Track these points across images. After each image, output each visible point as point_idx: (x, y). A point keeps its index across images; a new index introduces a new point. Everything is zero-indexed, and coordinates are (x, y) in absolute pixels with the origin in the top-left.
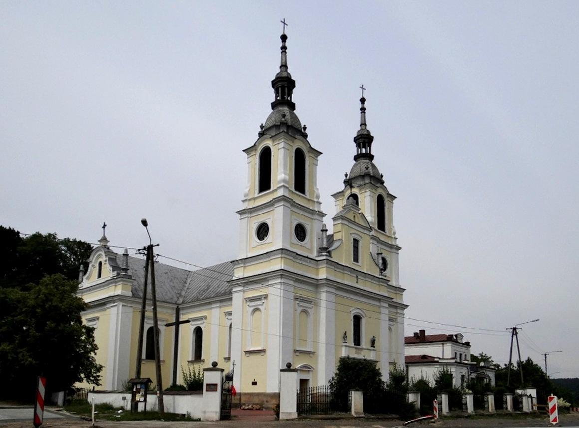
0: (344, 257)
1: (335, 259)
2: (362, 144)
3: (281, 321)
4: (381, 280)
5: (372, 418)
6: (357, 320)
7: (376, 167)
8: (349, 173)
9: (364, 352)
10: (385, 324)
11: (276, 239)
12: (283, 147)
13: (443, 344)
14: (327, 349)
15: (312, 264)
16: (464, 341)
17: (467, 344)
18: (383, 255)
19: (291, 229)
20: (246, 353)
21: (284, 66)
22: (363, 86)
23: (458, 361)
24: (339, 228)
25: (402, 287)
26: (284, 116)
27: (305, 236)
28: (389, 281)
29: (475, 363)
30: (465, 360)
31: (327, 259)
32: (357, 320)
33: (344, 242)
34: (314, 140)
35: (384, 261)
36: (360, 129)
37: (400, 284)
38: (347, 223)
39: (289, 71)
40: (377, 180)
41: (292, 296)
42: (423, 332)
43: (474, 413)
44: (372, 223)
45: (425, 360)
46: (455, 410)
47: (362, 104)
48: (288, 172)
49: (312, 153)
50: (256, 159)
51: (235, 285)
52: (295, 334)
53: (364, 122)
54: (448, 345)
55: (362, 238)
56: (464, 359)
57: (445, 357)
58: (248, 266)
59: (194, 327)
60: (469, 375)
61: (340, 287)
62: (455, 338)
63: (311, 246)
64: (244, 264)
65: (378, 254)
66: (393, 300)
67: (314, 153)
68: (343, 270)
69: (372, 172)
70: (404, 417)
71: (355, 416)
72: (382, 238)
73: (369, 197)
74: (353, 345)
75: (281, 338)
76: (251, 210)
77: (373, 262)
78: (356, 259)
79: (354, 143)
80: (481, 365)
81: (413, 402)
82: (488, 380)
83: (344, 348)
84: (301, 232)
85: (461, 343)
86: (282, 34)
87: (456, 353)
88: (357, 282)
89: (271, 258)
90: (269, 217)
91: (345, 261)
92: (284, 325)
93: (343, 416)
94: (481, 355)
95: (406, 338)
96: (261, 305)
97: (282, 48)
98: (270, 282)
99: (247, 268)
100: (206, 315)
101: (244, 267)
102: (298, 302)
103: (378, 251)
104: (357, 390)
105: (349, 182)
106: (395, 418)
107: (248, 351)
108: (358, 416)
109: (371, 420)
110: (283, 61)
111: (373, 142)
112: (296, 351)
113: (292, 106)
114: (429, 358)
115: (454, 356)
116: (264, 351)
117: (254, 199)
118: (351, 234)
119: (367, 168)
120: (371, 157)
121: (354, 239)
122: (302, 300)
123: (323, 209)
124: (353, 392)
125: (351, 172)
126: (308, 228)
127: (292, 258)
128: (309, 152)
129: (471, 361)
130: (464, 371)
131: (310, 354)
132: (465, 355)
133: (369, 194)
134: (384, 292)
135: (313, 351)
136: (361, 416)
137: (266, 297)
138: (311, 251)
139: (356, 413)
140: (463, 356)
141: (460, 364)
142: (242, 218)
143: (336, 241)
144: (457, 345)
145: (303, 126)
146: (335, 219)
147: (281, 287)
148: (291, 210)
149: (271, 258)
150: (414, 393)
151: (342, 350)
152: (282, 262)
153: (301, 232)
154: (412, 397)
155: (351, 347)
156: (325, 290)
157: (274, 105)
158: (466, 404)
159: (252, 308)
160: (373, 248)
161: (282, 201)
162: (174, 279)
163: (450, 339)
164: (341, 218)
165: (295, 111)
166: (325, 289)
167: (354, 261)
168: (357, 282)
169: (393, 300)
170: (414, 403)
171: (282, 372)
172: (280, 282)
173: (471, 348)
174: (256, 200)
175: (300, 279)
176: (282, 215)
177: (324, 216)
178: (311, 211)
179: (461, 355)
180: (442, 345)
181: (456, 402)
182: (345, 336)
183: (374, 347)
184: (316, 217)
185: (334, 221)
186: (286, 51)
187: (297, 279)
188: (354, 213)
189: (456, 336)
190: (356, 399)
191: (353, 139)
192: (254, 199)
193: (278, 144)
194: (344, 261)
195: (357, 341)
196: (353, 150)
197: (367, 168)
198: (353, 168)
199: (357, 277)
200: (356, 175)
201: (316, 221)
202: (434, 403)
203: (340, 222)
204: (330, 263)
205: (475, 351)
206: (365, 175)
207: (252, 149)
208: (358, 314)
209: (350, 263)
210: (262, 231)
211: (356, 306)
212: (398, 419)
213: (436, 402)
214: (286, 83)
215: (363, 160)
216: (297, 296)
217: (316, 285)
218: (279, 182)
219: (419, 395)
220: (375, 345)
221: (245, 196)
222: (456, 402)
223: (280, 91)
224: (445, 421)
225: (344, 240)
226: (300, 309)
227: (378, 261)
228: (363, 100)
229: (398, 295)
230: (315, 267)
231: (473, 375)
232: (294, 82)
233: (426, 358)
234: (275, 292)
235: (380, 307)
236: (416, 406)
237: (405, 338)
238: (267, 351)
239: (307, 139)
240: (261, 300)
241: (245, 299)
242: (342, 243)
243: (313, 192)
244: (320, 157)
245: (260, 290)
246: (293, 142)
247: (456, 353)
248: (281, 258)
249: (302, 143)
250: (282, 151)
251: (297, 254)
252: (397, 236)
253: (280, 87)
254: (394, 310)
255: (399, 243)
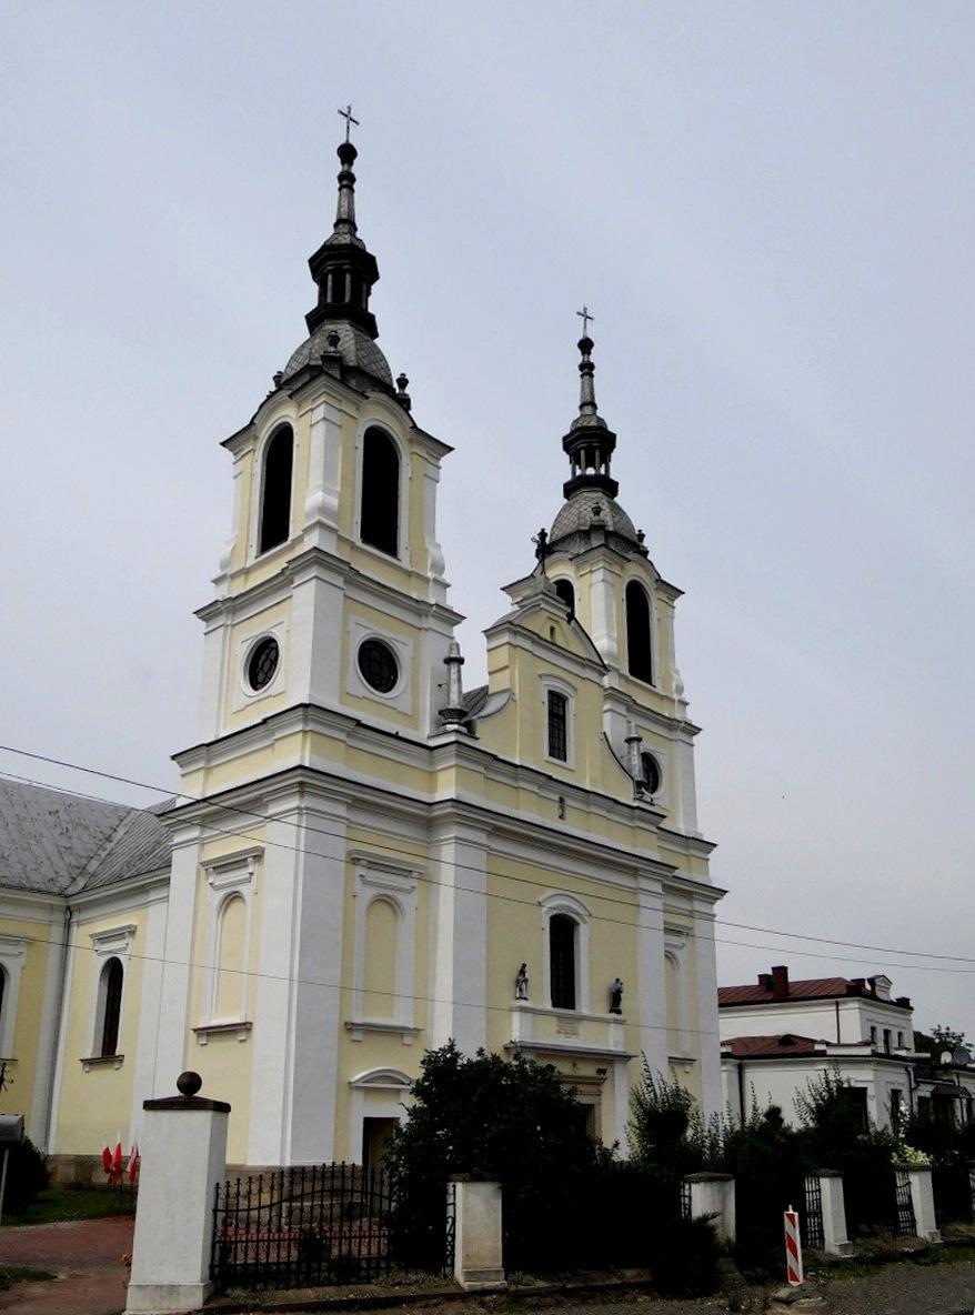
0: (516, 736)
1: (487, 739)
2: (582, 452)
3: (298, 929)
4: (637, 812)
5: (539, 1293)
6: (563, 931)
7: (624, 513)
8: (548, 531)
9: (583, 1027)
10: (652, 941)
11: (293, 683)
12: (324, 418)
13: (837, 1004)
14: (455, 1019)
15: (416, 759)
16: (893, 996)
17: (904, 1004)
18: (646, 746)
19: (344, 652)
20: (199, 1036)
21: (589, 403)
22: (585, 309)
23: (881, 1050)
24: (503, 656)
25: (705, 839)
26: (334, 340)
27: (396, 677)
28: (664, 817)
29: (928, 1055)
30: (901, 1047)
31: (457, 742)
32: (563, 931)
33: (517, 698)
34: (424, 414)
35: (649, 763)
36: (578, 415)
37: (700, 831)
38: (527, 644)
39: (358, 235)
40: (627, 544)
41: (340, 849)
42: (781, 972)
43: (939, 1241)
44: (610, 654)
45: (790, 1049)
46: (874, 1234)
47: (583, 354)
48: (339, 489)
49: (420, 444)
50: (254, 463)
51: (184, 821)
52: (346, 971)
53: (588, 399)
54: (850, 1005)
55: (576, 690)
56: (896, 1045)
57: (842, 1042)
58: (216, 766)
59: (104, 959)
60: (911, 1090)
61: (501, 828)
62: (868, 987)
63: (412, 707)
64: (208, 761)
65: (629, 741)
66: (677, 873)
67: (425, 446)
68: (516, 778)
69: (610, 523)
70: (669, 1285)
71: (466, 1285)
72: (643, 699)
73: (602, 584)
74: (548, 1005)
75: (296, 985)
76: (234, 605)
77: (612, 761)
78: (558, 748)
79: (565, 453)
80: (942, 1062)
81: (705, 1219)
82: (964, 1101)
83: (516, 1016)
84: (378, 665)
85: (887, 1002)
86: (343, 141)
87: (873, 1029)
88: (561, 817)
89: (277, 736)
90: (280, 620)
91: (520, 758)
92: (308, 941)
93: (413, 1291)
94: (938, 1034)
95: (722, 992)
96: (241, 882)
97: (341, 178)
98: (272, 810)
99: (216, 770)
100: (135, 923)
101: (208, 770)
102: (363, 871)
103: (630, 730)
104: (477, 1178)
105: (545, 549)
106: (634, 1286)
107: (204, 1029)
108: (478, 1285)
109: (534, 1301)
110: (345, 209)
111: (615, 450)
112: (350, 1027)
113: (368, 326)
114: (800, 1043)
115: (868, 1037)
116: (246, 1027)
117: (246, 572)
118: (540, 676)
119: (597, 511)
120: (610, 488)
121: (550, 693)
122: (376, 865)
123: (453, 601)
124: (459, 1186)
125: (554, 526)
126: (404, 655)
127: (342, 736)
128: (411, 441)
129: (917, 1051)
130: (899, 1079)
131: (402, 1035)
132: (900, 1034)
133: (602, 577)
134: (648, 848)
135: (412, 1026)
136: (488, 1284)
137: (258, 855)
138: (412, 718)
139: (469, 1275)
140: (894, 1037)
141: (885, 1059)
142: (213, 627)
143: (494, 694)
144: (872, 1005)
145: (395, 376)
146: (490, 633)
147: (300, 819)
148: (345, 596)
149: (277, 736)
150: (710, 1180)
151: (511, 1021)
152: (308, 746)
153: (378, 665)
154: (702, 1199)
155: (546, 1013)
156: (452, 835)
157: (314, 320)
158: (909, 1207)
159: (221, 894)
160: (614, 724)
161: (315, 567)
162: (75, 829)
163: (855, 989)
164: (509, 630)
165: (376, 341)
166: (453, 832)
167: (551, 754)
168: (561, 817)
169: (677, 873)
170: (712, 1222)
171: (151, 1114)
172: (298, 808)
173: (914, 1016)
174: (251, 577)
175: (365, 800)
176: (311, 609)
177: (458, 623)
178: (413, 604)
179: (887, 1033)
180: (834, 1008)
181: (874, 1206)
182: (521, 978)
183: (619, 1012)
184: (431, 623)
185: (488, 637)
186: (355, 186)
187: (356, 799)
188: (549, 618)
189: (872, 981)
190: (475, 1214)
191: (560, 445)
192: (246, 572)
193: (312, 410)
194: (517, 754)
195: (564, 993)
196: (563, 470)
197: (597, 511)
198: (560, 515)
199: (561, 800)
200: (569, 531)
201: (430, 633)
202: (787, 1221)
203: (506, 638)
204: (468, 752)
205: (924, 1021)
206: (595, 524)
207: (245, 436)
208: (564, 912)
209: (540, 759)
210: (262, 662)
211: (561, 887)
212: (644, 1288)
213: (791, 1217)
214: (347, 261)
215: (585, 494)
216: (358, 852)
217: (426, 819)
218: (308, 515)
219: (731, 1187)
220: (623, 1006)
221: (222, 568)
222: (874, 1206)
223: (330, 284)
224: (834, 1284)
225: (517, 692)
226: (369, 893)
227: (629, 760)
228: (586, 346)
229: (692, 859)
230: (425, 767)
231: (926, 1091)
232: (613, 436)
233: (793, 1043)
234: (282, 836)
235: (636, 891)
236: (719, 1231)
237: (719, 989)
238: (256, 1029)
239: (410, 412)
240: (246, 866)
241: (203, 864)
242: (511, 699)
243: (420, 553)
244: (445, 461)
245: (248, 834)
246: (622, 568)
247: (873, 1029)
248: (305, 732)
249: (389, 415)
250: (321, 429)
251: (359, 723)
252: (686, 696)
253: (330, 271)
254: (684, 904)
255: (693, 715)
